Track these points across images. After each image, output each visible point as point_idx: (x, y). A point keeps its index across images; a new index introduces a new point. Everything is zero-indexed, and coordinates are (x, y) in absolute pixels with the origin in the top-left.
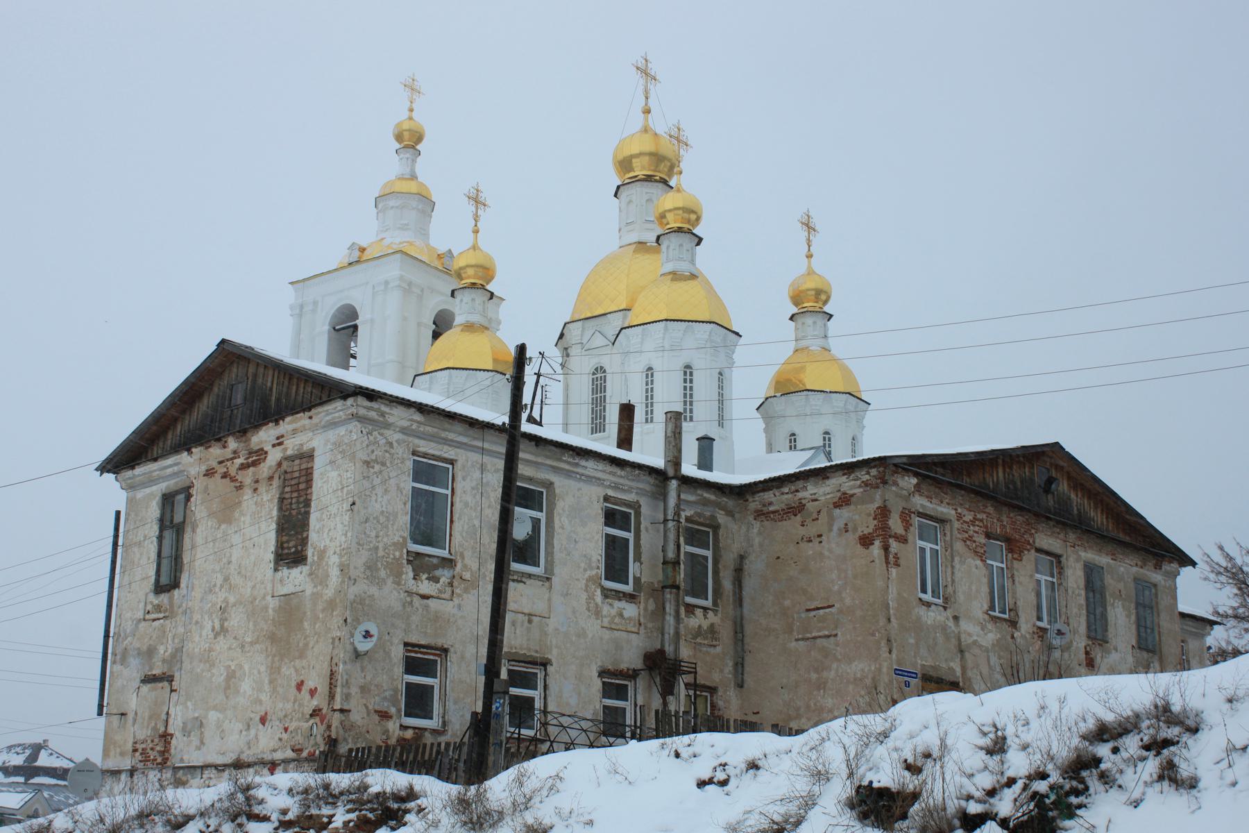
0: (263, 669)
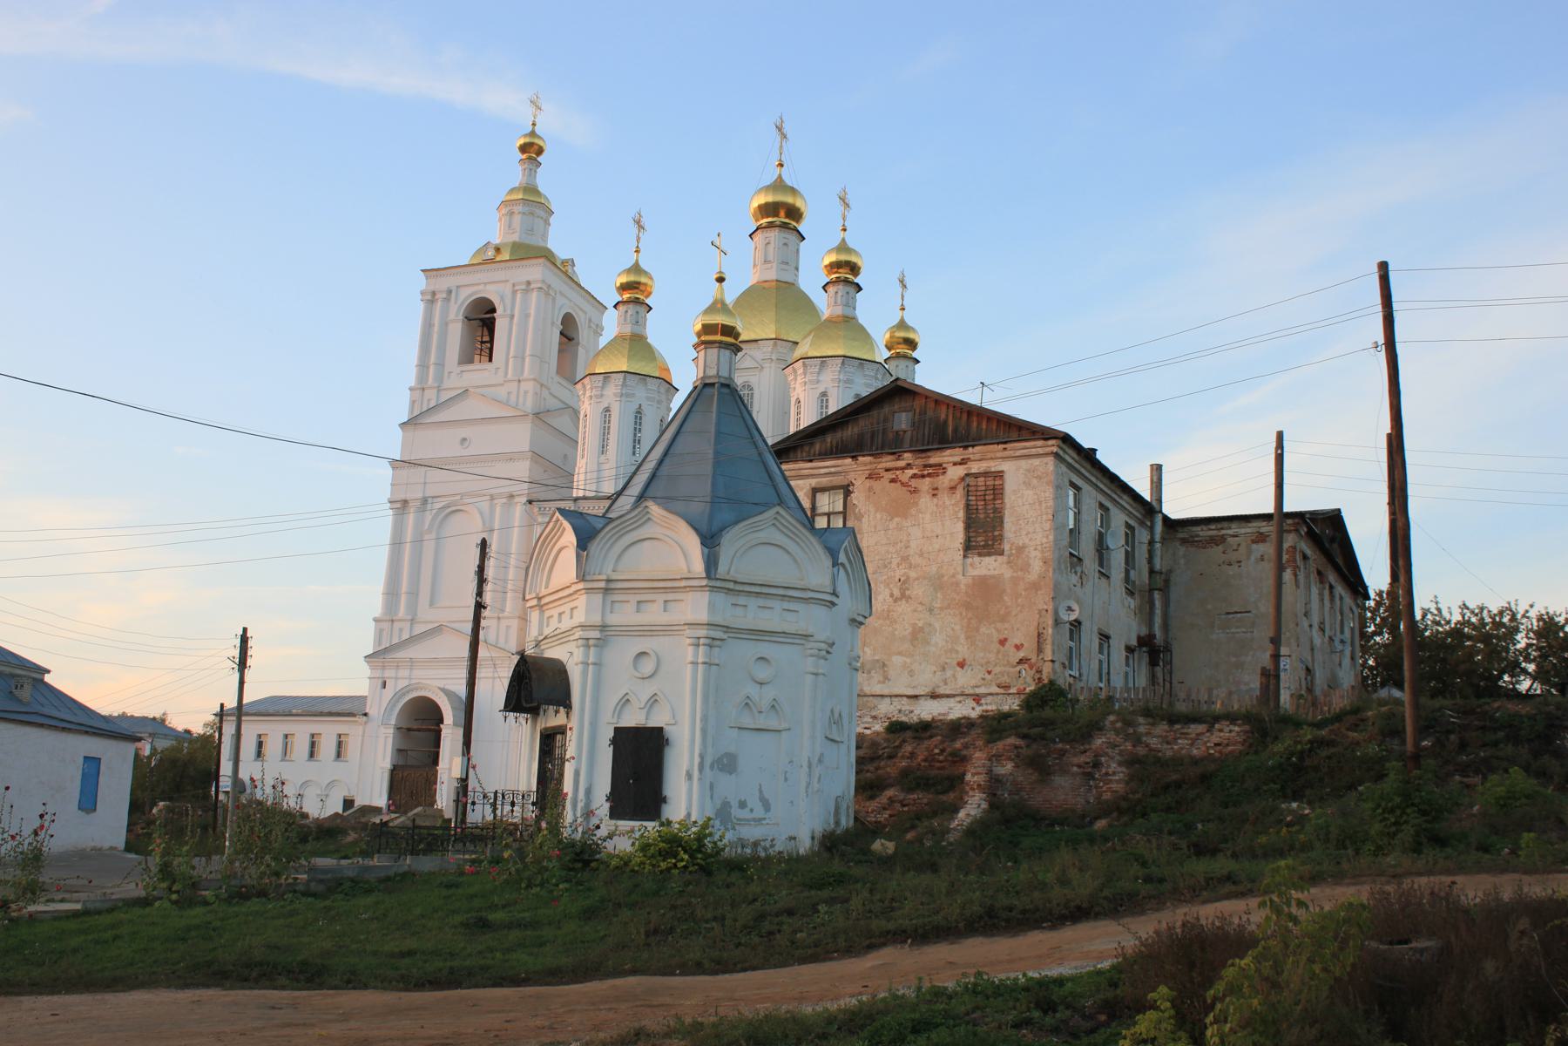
0: (957, 628)
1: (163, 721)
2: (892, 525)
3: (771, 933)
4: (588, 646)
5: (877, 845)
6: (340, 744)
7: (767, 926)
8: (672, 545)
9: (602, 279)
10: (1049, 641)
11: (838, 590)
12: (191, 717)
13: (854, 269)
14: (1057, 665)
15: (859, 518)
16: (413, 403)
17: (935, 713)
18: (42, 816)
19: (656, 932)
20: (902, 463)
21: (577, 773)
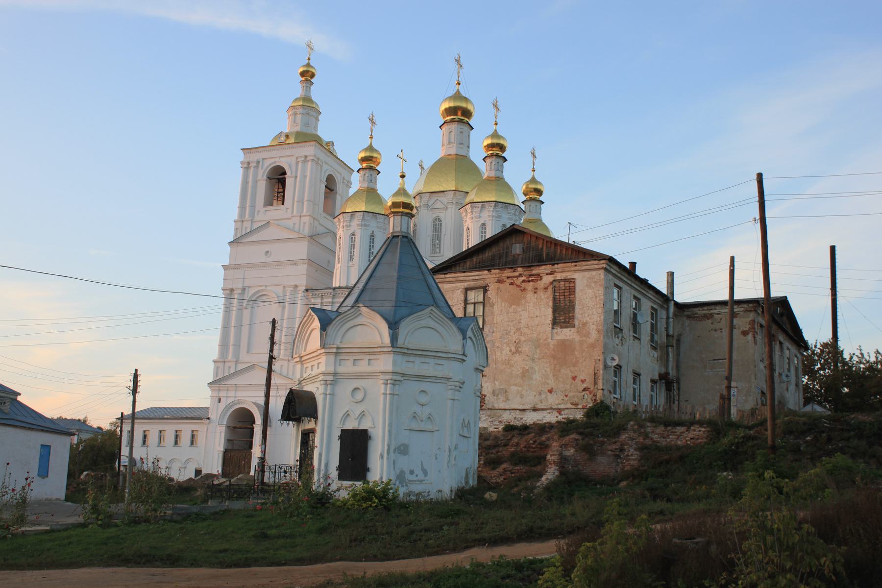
0: (548, 370)
1: (85, 421)
2: (511, 310)
3: (415, 541)
4: (326, 385)
5: (487, 496)
6: (193, 436)
7: (414, 537)
8: (372, 329)
9: (350, 154)
10: (601, 378)
11: (466, 352)
12: (102, 418)
13: (502, 148)
14: (605, 392)
15: (492, 305)
16: (236, 229)
17: (535, 420)
18: (27, 479)
19: (355, 540)
20: (517, 274)
21: (320, 455)
